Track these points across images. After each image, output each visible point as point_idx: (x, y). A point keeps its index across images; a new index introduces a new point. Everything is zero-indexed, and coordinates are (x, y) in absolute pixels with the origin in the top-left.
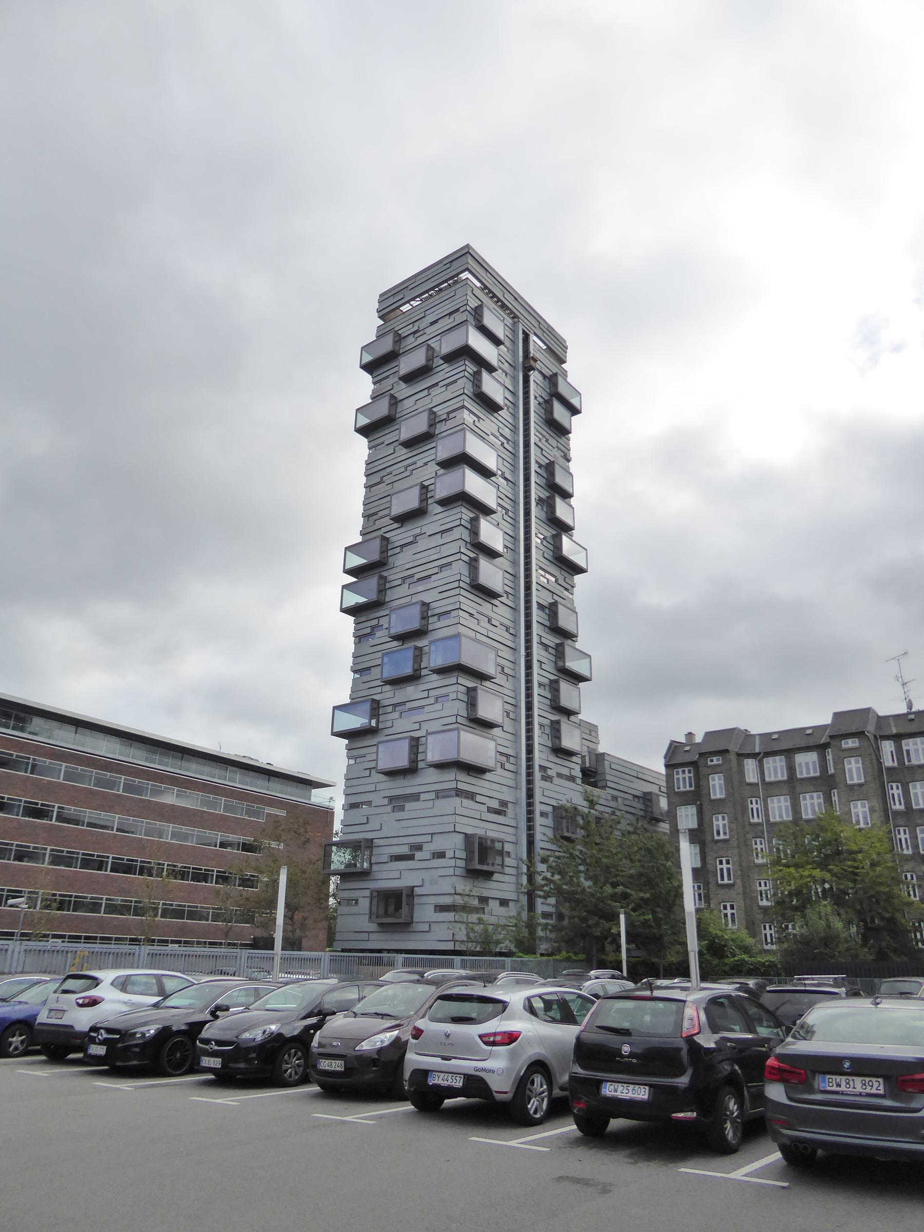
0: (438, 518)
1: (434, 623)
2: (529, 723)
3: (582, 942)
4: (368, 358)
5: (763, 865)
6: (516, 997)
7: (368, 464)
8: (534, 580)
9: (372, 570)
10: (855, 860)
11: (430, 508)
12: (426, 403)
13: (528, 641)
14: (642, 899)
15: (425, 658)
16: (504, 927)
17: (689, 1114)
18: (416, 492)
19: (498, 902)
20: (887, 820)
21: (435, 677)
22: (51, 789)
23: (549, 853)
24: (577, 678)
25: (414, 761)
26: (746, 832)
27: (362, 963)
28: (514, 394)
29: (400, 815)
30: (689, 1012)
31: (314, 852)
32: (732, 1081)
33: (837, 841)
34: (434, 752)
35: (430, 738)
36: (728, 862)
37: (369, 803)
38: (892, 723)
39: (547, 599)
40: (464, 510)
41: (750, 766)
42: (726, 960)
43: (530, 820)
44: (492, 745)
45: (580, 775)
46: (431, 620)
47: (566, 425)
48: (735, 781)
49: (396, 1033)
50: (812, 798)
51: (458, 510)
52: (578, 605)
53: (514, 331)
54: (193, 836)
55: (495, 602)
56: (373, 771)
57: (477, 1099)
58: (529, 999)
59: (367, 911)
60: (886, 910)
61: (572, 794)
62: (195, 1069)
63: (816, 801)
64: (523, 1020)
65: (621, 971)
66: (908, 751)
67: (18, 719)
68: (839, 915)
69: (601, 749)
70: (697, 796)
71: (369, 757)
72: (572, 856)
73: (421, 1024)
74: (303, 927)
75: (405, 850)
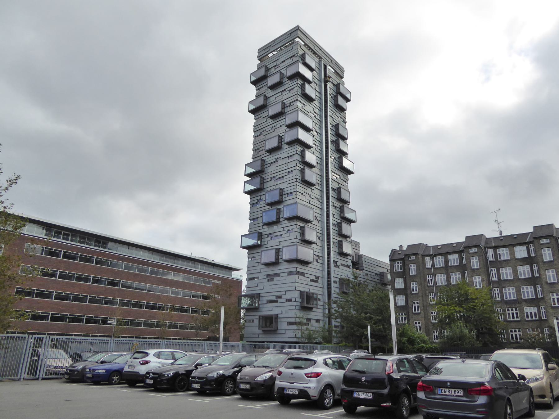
0: (286, 151)
1: (285, 198)
2: (328, 242)
3: (351, 337)
4: (254, 79)
5: (433, 304)
6: (319, 359)
7: (254, 127)
8: (330, 178)
9: (257, 174)
10: (474, 302)
11: (283, 146)
12: (280, 99)
13: (328, 205)
14: (378, 319)
15: (282, 213)
16: (318, 332)
17: (388, 404)
18: (276, 139)
19: (315, 321)
20: (489, 284)
21: (286, 222)
22: (119, 273)
23: (337, 299)
24: (350, 221)
25: (277, 259)
26: (425, 290)
27: (258, 347)
28: (320, 93)
29: (271, 283)
30: (389, 364)
31: (234, 299)
32: (406, 392)
33: (466, 294)
34: (286, 255)
35: (284, 249)
36: (417, 303)
37: (258, 278)
38: (493, 241)
39: (336, 186)
40: (298, 147)
41: (428, 260)
42: (415, 346)
43: (329, 284)
44: (312, 252)
45: (351, 264)
46: (284, 196)
47: (344, 107)
48: (421, 267)
49: (271, 374)
50: (456, 275)
51: (295, 147)
52: (350, 188)
53: (320, 65)
54: (181, 293)
55: (313, 188)
56: (259, 264)
57: (304, 400)
58: (325, 360)
59: (258, 325)
60: (488, 325)
61: (347, 273)
62: (189, 389)
63: (457, 276)
64: (324, 367)
65: (368, 351)
66: (499, 254)
67: (103, 243)
68: (467, 327)
69: (361, 253)
70: (404, 274)
71: (257, 258)
72: (347, 301)
73: (281, 369)
74: (230, 332)
75: (274, 298)
